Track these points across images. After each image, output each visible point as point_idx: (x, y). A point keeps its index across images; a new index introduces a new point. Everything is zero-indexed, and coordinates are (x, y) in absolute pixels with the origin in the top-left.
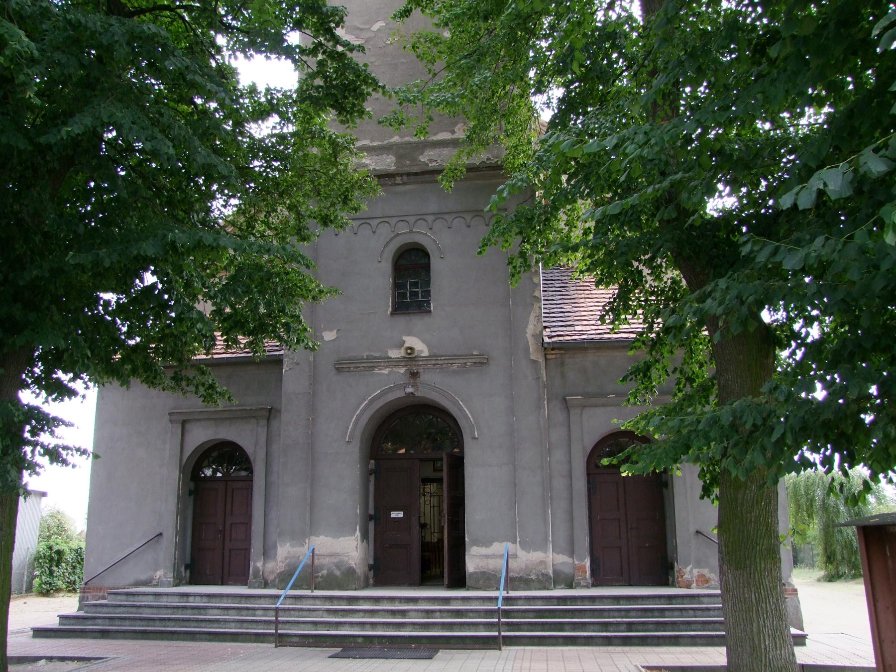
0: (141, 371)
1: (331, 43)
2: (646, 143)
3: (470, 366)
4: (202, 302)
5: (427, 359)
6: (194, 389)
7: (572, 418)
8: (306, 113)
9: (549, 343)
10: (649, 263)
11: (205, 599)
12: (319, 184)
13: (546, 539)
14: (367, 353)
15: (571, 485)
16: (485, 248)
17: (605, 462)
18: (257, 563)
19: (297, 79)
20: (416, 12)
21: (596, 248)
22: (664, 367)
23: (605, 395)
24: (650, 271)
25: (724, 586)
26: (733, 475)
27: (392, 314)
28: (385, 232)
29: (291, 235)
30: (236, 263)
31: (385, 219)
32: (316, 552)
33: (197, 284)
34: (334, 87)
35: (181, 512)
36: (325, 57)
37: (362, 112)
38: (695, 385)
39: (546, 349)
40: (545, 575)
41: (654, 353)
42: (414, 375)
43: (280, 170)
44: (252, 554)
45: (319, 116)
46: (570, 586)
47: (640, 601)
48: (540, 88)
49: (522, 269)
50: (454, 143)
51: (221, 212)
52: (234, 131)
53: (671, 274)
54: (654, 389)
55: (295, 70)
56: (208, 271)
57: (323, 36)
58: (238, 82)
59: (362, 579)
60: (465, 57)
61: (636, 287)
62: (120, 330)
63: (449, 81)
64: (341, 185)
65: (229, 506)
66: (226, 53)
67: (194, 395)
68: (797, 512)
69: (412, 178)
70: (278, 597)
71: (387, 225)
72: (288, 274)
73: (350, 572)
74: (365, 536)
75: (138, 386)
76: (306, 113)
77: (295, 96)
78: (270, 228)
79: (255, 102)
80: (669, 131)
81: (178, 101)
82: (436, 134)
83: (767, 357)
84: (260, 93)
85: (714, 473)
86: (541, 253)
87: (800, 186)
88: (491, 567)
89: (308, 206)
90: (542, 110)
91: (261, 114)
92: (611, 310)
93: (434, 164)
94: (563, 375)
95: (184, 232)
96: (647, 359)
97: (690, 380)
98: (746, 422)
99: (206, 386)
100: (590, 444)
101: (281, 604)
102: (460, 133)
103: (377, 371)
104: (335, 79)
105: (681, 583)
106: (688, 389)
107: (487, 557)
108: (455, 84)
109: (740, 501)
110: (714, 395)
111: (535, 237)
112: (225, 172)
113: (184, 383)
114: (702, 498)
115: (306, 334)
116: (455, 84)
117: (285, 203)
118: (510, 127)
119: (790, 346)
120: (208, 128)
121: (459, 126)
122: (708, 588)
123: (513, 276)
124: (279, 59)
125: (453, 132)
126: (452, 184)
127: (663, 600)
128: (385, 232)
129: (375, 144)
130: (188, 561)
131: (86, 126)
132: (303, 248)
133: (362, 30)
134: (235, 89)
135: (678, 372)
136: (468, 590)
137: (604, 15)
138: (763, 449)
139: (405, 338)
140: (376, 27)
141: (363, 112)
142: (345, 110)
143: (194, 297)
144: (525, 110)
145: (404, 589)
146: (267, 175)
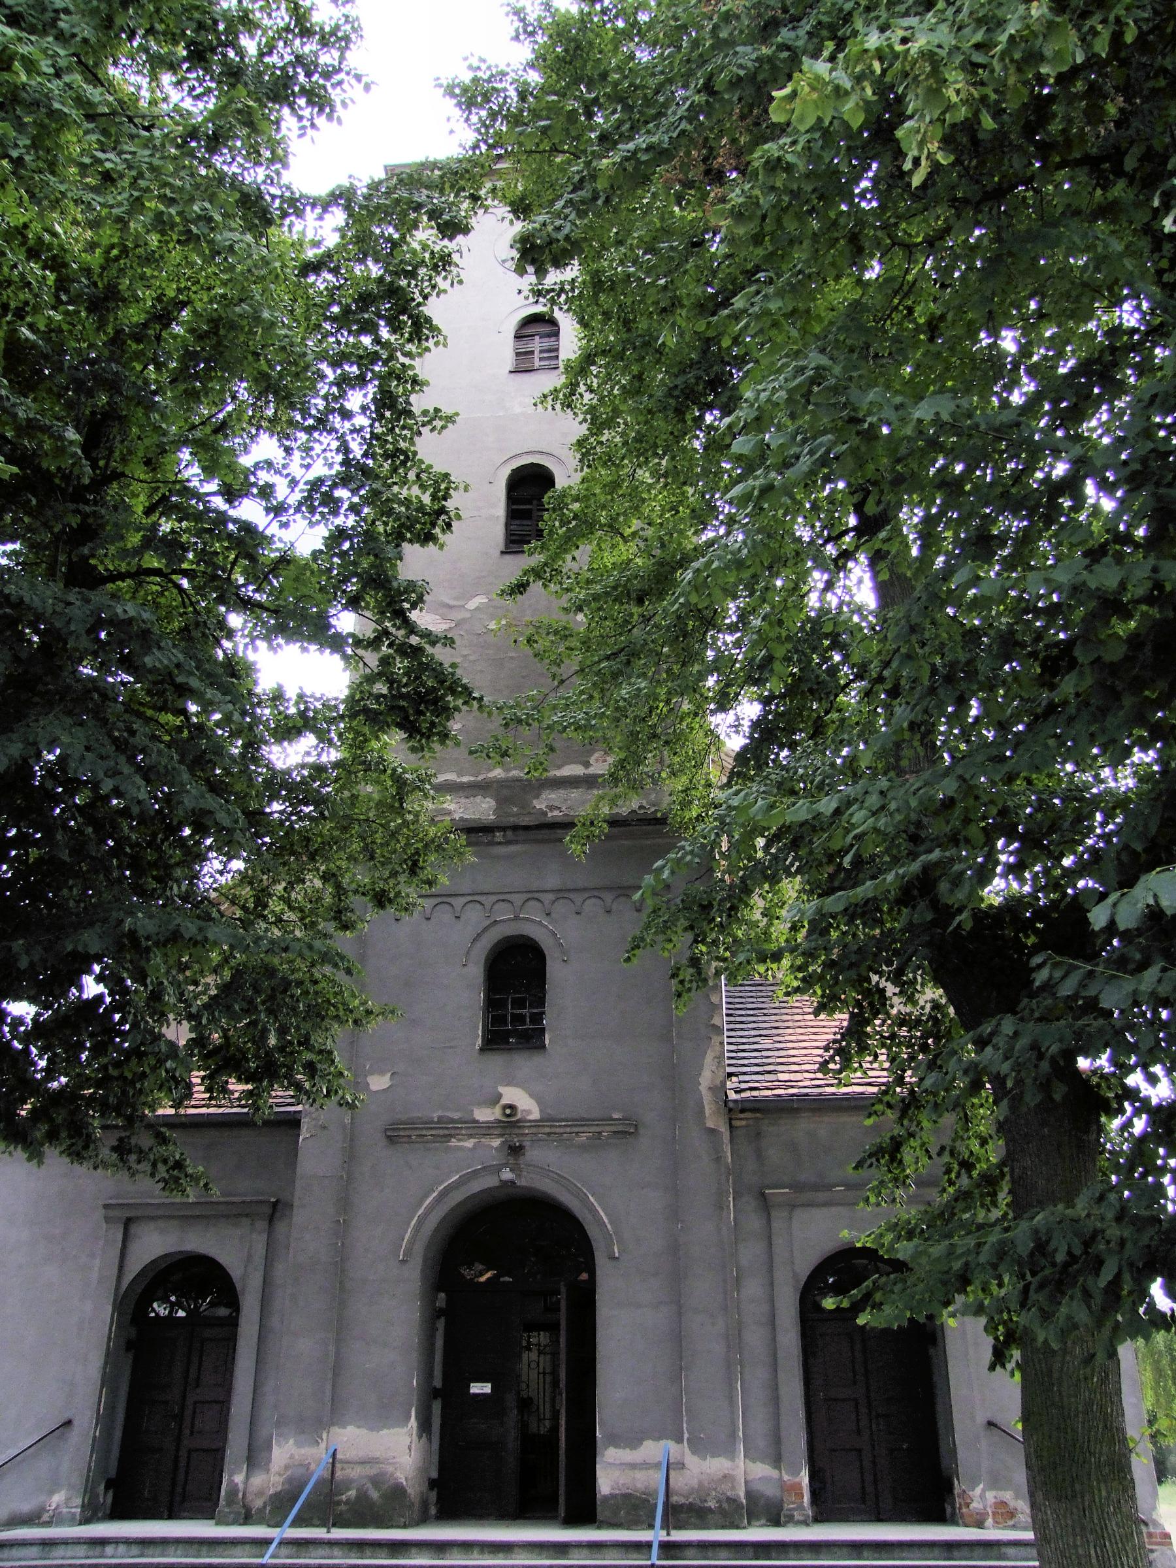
0: (64, 1134)
1: (402, 632)
2: (883, 807)
3: (608, 1138)
4: (173, 1024)
5: (536, 1124)
6: (149, 1169)
7: (776, 1225)
8: (358, 733)
9: (735, 1101)
10: (896, 977)
11: (135, 1550)
12: (373, 842)
13: (733, 1435)
14: (440, 1113)
15: (774, 1339)
16: (636, 952)
17: (829, 1303)
18: (235, 1477)
19: (347, 683)
20: (536, 587)
21: (810, 955)
22: (923, 1144)
23: (829, 1187)
24: (897, 990)
25: (1038, 1525)
26: (1041, 1339)
27: (482, 1050)
28: (474, 917)
29: (325, 920)
30: (233, 962)
31: (475, 897)
32: (339, 1456)
33: (170, 998)
34: (402, 696)
35: (108, 1380)
36: (390, 651)
37: (444, 736)
38: (975, 1173)
39: (733, 1111)
40: (732, 1501)
41: (906, 1122)
42: (515, 1150)
43: (312, 819)
44: (227, 1459)
45: (378, 738)
46: (776, 1522)
47: (897, 1552)
48: (724, 702)
49: (694, 985)
50: (590, 782)
51: (215, 881)
52: (243, 755)
53: (931, 994)
54: (908, 1181)
55: (344, 670)
56: (188, 973)
57: (390, 620)
58: (256, 683)
59: (417, 1506)
60: (608, 658)
61: (875, 1015)
62: (35, 1064)
63: (582, 693)
64: (408, 844)
65: (195, 1360)
66: (241, 641)
67: (148, 1178)
68: (1157, 1383)
69: (522, 835)
70: (266, 1542)
71: (478, 906)
72: (316, 982)
73: (397, 1493)
74: (425, 1426)
75: (55, 1160)
76: (358, 733)
77: (342, 707)
78: (291, 908)
79: (280, 713)
80: (918, 789)
81: (163, 709)
82: (559, 767)
83: (1087, 1132)
84: (288, 700)
85: (1011, 1325)
86: (725, 960)
87: (1118, 894)
88: (639, 1485)
89: (355, 875)
90: (728, 735)
91: (288, 731)
92: (839, 1052)
93: (556, 813)
94: (759, 1155)
95: (151, 917)
96: (896, 1132)
97: (967, 1166)
98: (1056, 1250)
99: (171, 1163)
100: (805, 1265)
101: (272, 1556)
102: (600, 765)
103: (454, 1142)
104: (405, 685)
105: (968, 1520)
106: (964, 1181)
107: (633, 1466)
108: (591, 697)
109: (1055, 1375)
110: (1006, 1189)
111: (714, 935)
112: (226, 822)
113: (133, 1158)
114: (992, 1368)
115: (342, 1081)
116: (591, 697)
117: (318, 870)
118: (677, 759)
119: (1122, 1111)
120: (204, 752)
121: (596, 755)
122: (1014, 1527)
123: (679, 995)
124: (321, 651)
125: (587, 765)
126: (587, 849)
127: (936, 1551)
128: (474, 917)
129: (465, 779)
130: (113, 1473)
131: (11, 758)
132: (343, 942)
133: (451, 607)
134: (250, 693)
135: (947, 1153)
136: (599, 1528)
137: (820, 600)
138: (1087, 1295)
139: (501, 1089)
140: (473, 604)
141: (446, 736)
142: (419, 731)
143: (162, 1017)
144: (701, 734)
145: (490, 1525)
146: (291, 827)
